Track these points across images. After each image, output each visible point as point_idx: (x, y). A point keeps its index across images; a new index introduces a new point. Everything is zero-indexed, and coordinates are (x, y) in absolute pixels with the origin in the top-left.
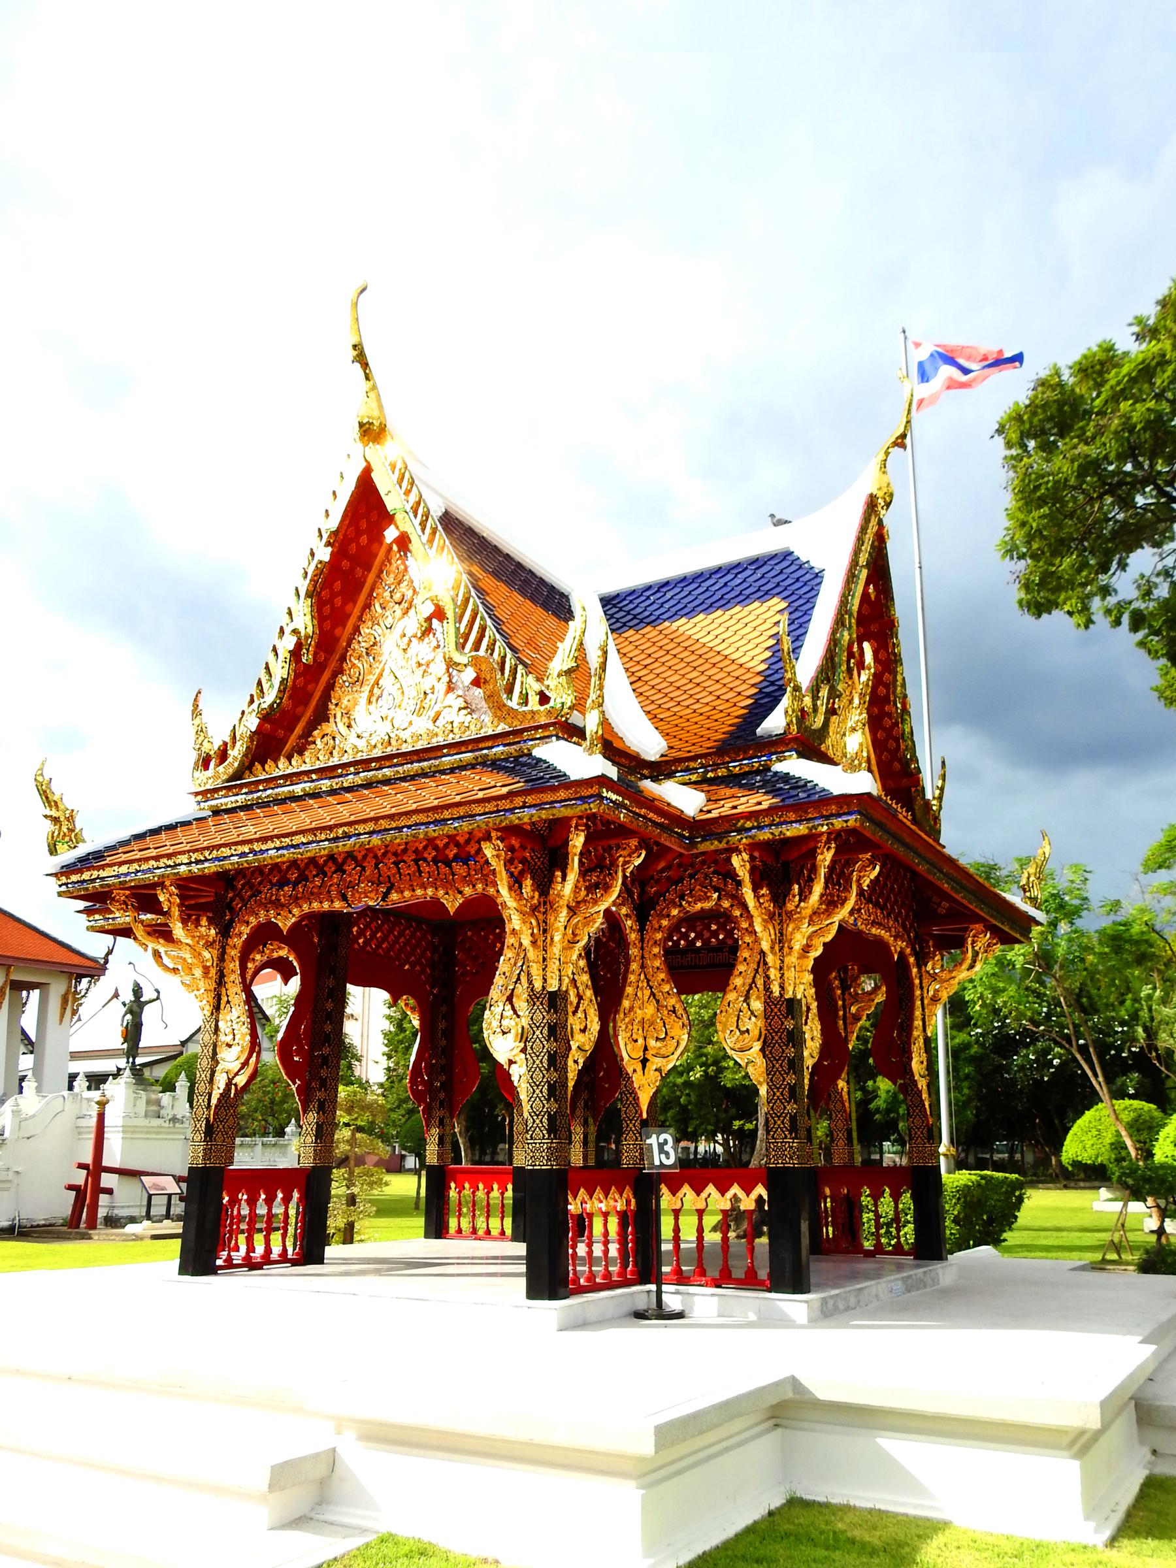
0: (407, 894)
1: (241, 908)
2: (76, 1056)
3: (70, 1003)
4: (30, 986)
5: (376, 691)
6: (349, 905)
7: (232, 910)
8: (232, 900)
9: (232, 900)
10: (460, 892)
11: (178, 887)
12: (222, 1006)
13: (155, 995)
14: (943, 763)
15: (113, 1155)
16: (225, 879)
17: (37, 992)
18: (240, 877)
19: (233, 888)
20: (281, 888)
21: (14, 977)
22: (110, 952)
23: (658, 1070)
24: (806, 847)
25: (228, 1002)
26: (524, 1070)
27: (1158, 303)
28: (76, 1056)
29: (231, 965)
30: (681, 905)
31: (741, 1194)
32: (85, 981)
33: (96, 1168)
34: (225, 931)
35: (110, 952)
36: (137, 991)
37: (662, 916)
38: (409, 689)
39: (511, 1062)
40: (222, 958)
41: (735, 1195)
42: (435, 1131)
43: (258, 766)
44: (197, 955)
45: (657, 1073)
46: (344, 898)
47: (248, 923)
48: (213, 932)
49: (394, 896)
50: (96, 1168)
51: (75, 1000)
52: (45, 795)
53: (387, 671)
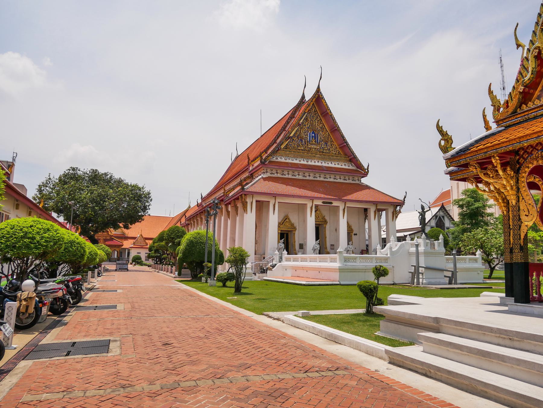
1: (524, 162)
2: (399, 231)
3: (395, 214)
4: (384, 210)
7: (519, 163)
8: (519, 159)
9: (519, 159)
11: (498, 157)
13: (428, 209)
15: (422, 264)
16: (516, 152)
17: (384, 212)
18: (521, 150)
19: (519, 155)
21: (378, 207)
22: (405, 197)
25: (523, 199)
27: (149, 194)
28: (399, 231)
29: (523, 185)
32: (398, 208)
33: (417, 267)
34: (517, 172)
35: (405, 197)
36: (423, 208)
40: (517, 182)
43: (524, 106)
44: (508, 182)
48: (512, 173)
50: (417, 267)
51: (396, 213)
52: (440, 129)
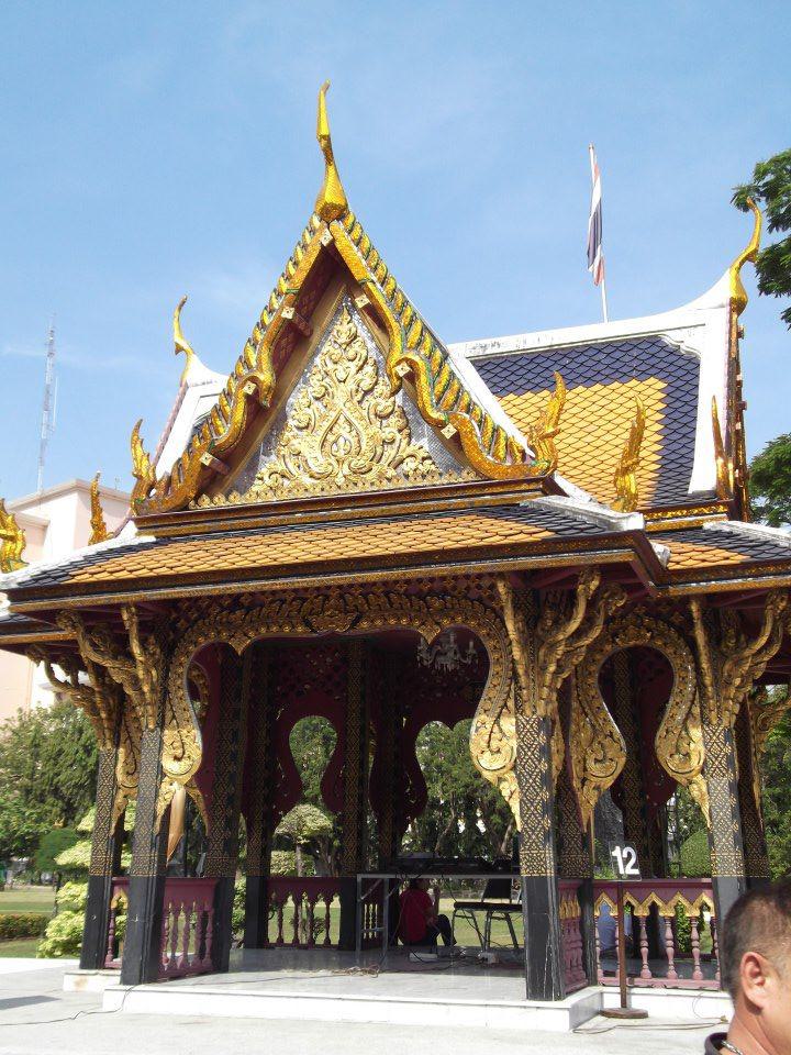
0: (404, 621)
5: (331, 438)
6: (313, 631)
7: (175, 630)
9: (177, 620)
10: (438, 624)
12: (167, 721)
14: (138, 426)
20: (232, 611)
23: (597, 788)
24: (571, 576)
25: (174, 717)
26: (515, 786)
30: (614, 642)
31: (685, 903)
37: (202, 634)
38: (340, 431)
39: (500, 780)
41: (654, 903)
42: (519, 829)
45: (596, 793)
46: (308, 624)
47: (196, 643)
49: (365, 624)
53: (342, 419)
